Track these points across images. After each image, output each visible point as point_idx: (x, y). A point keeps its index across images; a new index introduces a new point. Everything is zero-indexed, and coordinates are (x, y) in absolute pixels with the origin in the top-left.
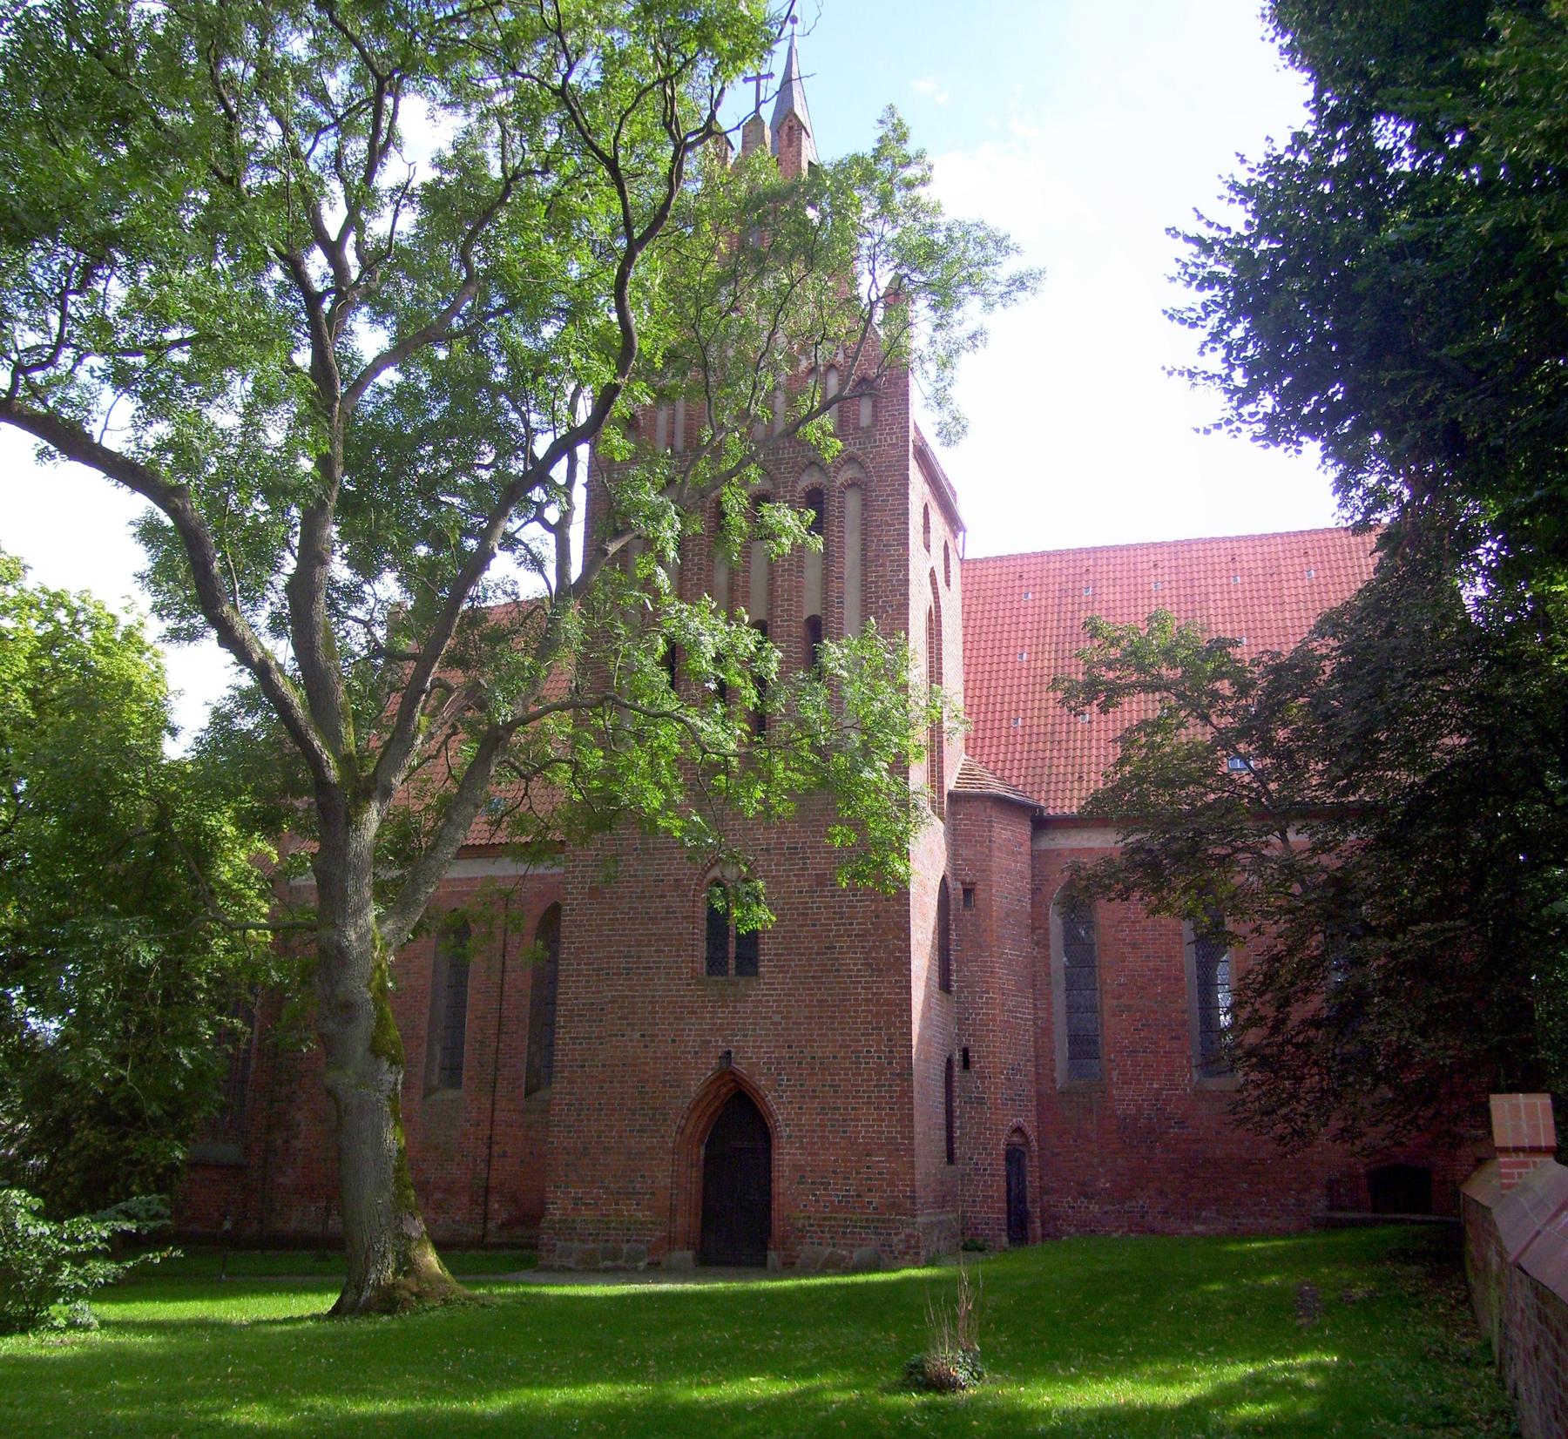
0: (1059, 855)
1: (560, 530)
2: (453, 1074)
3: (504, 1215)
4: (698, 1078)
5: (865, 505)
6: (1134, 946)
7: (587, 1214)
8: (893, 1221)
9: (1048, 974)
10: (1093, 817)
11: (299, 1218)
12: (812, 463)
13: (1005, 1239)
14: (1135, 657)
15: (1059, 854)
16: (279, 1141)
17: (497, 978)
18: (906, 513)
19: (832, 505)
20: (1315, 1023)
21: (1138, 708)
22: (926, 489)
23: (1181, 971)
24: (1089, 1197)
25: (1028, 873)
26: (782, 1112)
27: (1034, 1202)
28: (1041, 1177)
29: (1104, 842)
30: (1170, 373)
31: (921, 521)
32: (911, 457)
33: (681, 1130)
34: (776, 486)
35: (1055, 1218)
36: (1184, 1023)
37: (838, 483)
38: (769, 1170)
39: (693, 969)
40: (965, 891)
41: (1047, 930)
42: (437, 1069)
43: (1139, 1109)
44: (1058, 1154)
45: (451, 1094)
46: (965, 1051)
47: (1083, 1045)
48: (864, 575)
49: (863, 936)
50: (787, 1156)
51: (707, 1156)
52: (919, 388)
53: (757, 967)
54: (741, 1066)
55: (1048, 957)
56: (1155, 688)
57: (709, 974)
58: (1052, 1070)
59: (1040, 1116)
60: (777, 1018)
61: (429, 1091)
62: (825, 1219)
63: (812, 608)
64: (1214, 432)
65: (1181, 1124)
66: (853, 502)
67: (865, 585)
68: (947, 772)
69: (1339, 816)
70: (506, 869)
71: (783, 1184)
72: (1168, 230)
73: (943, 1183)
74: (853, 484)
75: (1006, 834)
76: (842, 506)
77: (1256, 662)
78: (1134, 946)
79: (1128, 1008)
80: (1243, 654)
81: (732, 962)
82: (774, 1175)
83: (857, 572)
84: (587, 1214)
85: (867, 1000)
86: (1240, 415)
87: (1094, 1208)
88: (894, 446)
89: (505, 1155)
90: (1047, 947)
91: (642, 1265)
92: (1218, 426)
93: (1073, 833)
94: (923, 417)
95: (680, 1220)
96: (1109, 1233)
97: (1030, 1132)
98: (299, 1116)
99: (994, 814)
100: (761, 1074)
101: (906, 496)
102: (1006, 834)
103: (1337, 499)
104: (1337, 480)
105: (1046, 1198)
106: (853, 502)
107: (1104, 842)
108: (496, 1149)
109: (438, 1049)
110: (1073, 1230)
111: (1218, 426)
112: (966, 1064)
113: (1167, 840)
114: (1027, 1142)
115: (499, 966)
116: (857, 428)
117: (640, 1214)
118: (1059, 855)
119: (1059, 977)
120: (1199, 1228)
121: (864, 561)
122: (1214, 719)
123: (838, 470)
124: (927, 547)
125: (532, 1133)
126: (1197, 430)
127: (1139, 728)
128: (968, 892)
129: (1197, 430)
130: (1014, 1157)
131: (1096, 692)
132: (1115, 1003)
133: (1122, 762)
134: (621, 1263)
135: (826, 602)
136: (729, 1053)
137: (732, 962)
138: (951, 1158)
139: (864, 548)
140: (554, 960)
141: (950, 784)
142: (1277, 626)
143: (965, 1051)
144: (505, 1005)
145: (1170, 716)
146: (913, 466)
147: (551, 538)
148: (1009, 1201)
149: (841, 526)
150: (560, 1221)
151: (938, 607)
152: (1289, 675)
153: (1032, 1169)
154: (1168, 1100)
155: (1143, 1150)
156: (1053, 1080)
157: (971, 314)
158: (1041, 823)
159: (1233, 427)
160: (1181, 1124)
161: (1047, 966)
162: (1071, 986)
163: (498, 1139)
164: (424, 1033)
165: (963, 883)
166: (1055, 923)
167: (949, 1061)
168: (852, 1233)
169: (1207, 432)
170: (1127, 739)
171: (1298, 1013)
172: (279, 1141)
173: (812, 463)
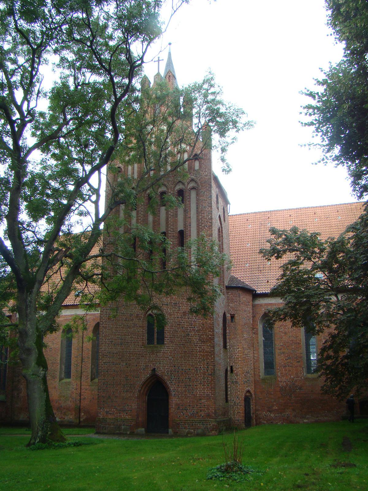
0: (261, 306)
1: (96, 203)
2: (68, 374)
3: (85, 417)
4: (145, 376)
5: (197, 195)
6: (285, 333)
7: (110, 416)
8: (209, 420)
9: (258, 343)
10: (274, 293)
11: (22, 417)
12: (180, 182)
13: (244, 425)
14: (288, 241)
15: (261, 305)
16: (16, 394)
17: (81, 345)
18: (211, 196)
19: (186, 195)
20: (346, 357)
21: (289, 257)
22: (217, 190)
23: (300, 341)
24: (271, 412)
25: (251, 311)
26: (172, 387)
27: (253, 414)
28: (256, 406)
29: (278, 302)
30: (301, 146)
31: (215, 199)
32: (212, 179)
33: (140, 391)
34: (168, 189)
35: (260, 418)
36: (301, 357)
37: (188, 188)
38: (168, 406)
39: (143, 343)
40: (231, 317)
41: (257, 329)
42: (63, 373)
43: (287, 384)
44: (261, 399)
45: (68, 380)
46: (231, 367)
47: (269, 365)
48: (198, 217)
49: (198, 331)
50: (174, 401)
51: (148, 399)
52: (215, 155)
53: (164, 342)
54: (159, 373)
55: (258, 337)
56: (294, 250)
57: (148, 344)
58: (259, 372)
59: (255, 387)
60: (170, 358)
61: (61, 379)
62: (186, 420)
63: (180, 227)
64: (318, 164)
65: (300, 388)
66: (193, 194)
67: (198, 220)
68: (225, 279)
69: (355, 290)
70: (80, 312)
71: (172, 410)
72: (320, 69)
73: (224, 408)
74: (193, 188)
75: (245, 299)
76: (190, 195)
77: (326, 242)
78: (285, 333)
79: (283, 353)
80: (322, 238)
81: (156, 340)
82: (170, 407)
83: (195, 216)
84: (110, 416)
85: (200, 351)
86: (326, 157)
87: (272, 415)
88: (206, 176)
89: (85, 398)
90: (257, 334)
91: (128, 433)
92: (319, 162)
93: (266, 299)
94: (216, 167)
95: (140, 419)
96: (277, 423)
97: (252, 391)
98: (22, 386)
99: (240, 292)
100: (165, 375)
101: (211, 191)
102: (245, 299)
103: (352, 188)
104: (352, 182)
105: (257, 412)
106: (193, 194)
107: (278, 302)
108: (82, 397)
109: (63, 367)
110: (265, 422)
111: (319, 162)
112: (232, 371)
113: (298, 300)
114: (251, 395)
115: (82, 342)
116: (194, 170)
117: (127, 417)
118: (261, 306)
119: (261, 343)
120: (305, 421)
121: (198, 212)
122: (312, 259)
123: (188, 184)
124: (218, 208)
125: (93, 392)
126: (313, 164)
127: (289, 264)
128: (233, 317)
129: (313, 164)
130: (247, 400)
131: (276, 253)
132: (279, 351)
133: (283, 275)
134: (122, 431)
135: (185, 225)
136: (155, 369)
137: (156, 340)
138: (227, 401)
139: (197, 208)
140: (98, 339)
141: (226, 283)
142: (330, 231)
143: (231, 367)
144: (84, 353)
145: (298, 260)
146: (213, 181)
147: (93, 205)
148: (245, 413)
149: (190, 201)
150: (102, 419)
151: (222, 228)
152: (337, 246)
153: (252, 403)
154: (296, 381)
155: (288, 397)
156: (260, 376)
157: (231, 133)
158: (255, 295)
159: (325, 161)
160: (300, 388)
161: (257, 340)
162: (265, 345)
163: (83, 394)
164: (59, 362)
165: (231, 315)
166: (260, 327)
167: (226, 370)
168: (195, 424)
169: (316, 164)
170: (285, 268)
171: (341, 354)
172: (16, 394)
173: (180, 182)
